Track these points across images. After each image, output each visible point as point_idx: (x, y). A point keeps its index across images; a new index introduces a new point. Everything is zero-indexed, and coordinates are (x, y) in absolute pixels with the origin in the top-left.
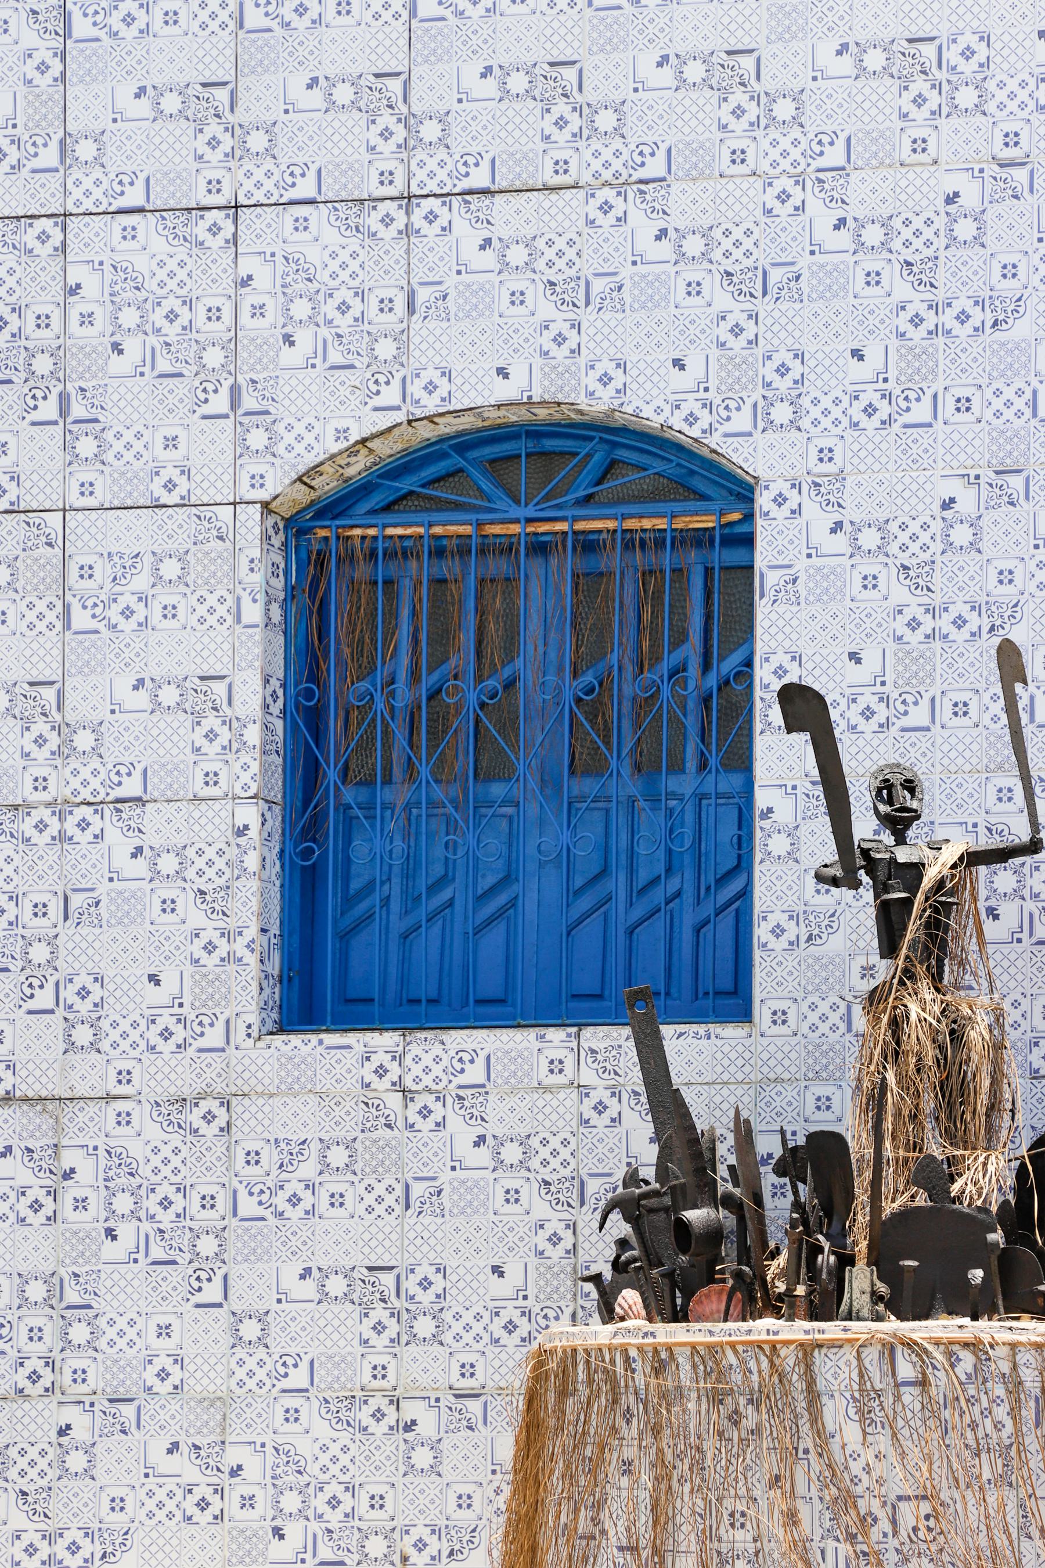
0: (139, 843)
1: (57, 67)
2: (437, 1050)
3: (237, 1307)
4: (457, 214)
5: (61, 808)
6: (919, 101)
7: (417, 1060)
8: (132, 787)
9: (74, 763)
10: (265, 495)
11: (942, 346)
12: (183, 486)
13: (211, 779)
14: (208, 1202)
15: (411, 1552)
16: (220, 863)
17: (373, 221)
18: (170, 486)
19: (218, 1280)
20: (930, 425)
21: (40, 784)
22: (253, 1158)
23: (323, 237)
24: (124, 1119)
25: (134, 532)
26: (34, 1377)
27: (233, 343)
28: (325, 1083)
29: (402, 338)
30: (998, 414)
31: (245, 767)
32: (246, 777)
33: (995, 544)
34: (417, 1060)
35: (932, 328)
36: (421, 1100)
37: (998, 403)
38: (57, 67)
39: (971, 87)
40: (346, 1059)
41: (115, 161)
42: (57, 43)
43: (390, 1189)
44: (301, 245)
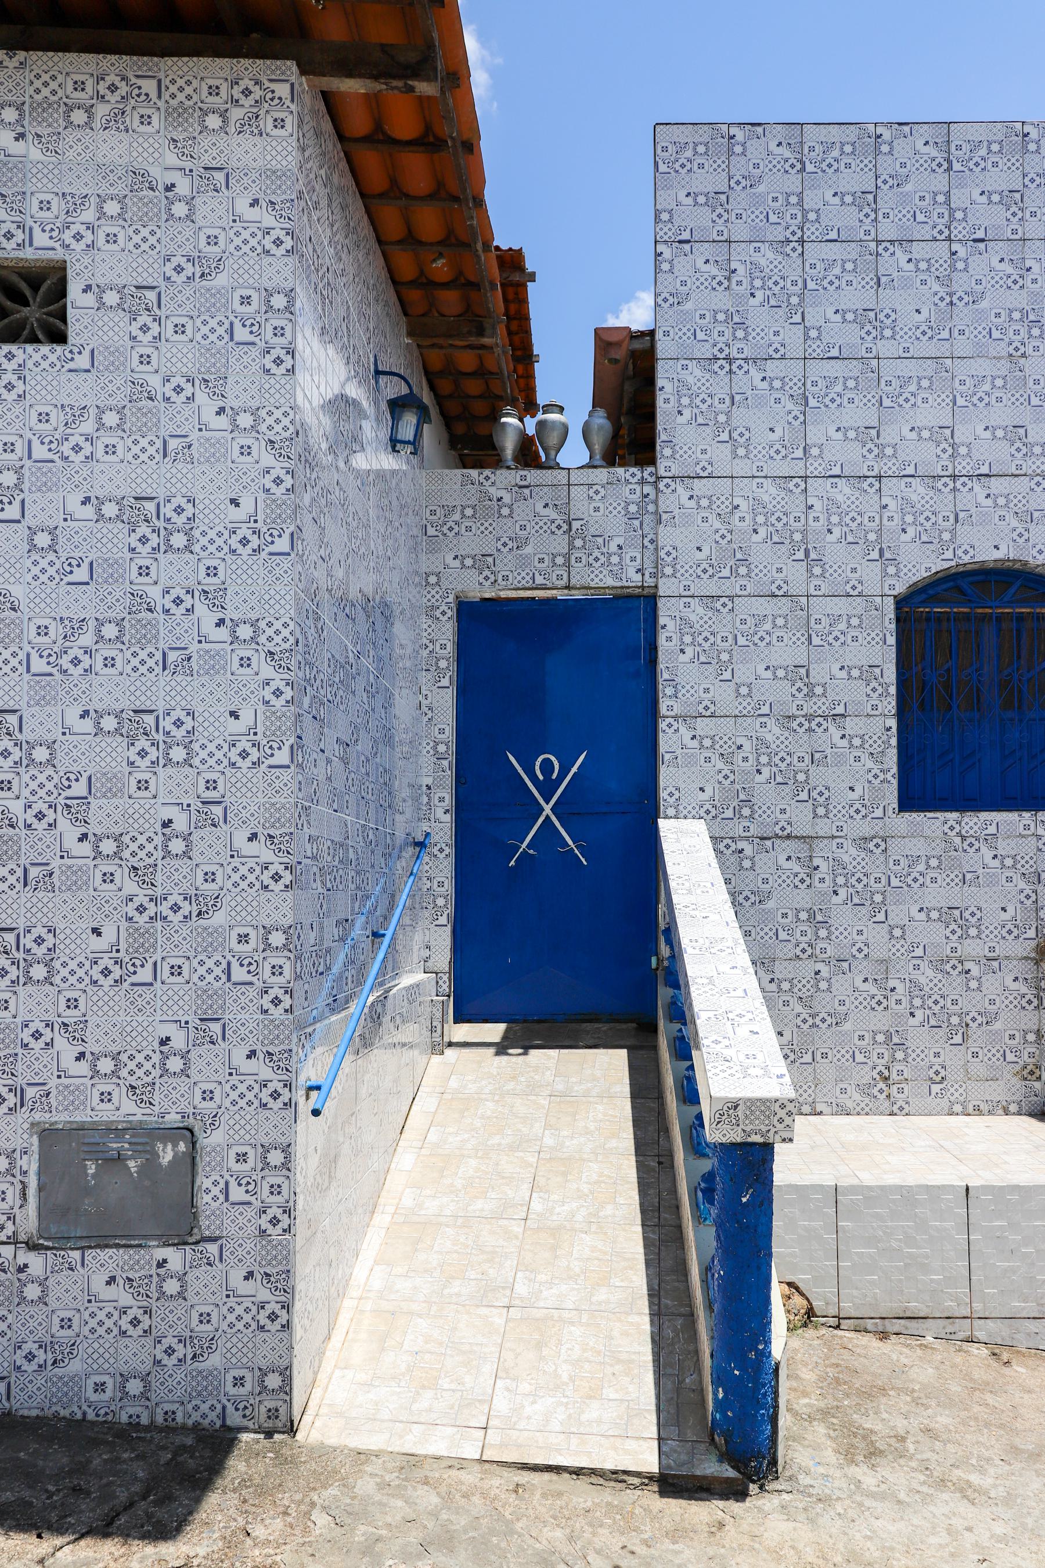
0: (82, 1049)
1: (802, 418)
2: (975, 820)
3: (891, 923)
5: (809, 718)
8: (840, 710)
9: (814, 699)
10: (895, 593)
11: (160, 928)
12: (860, 588)
13: (875, 707)
14: (878, 880)
16: (879, 742)
17: (940, 485)
18: (854, 588)
20: (151, 984)
21: (800, 707)
22: (897, 863)
23: (918, 491)
26: (804, 951)
27: (879, 531)
28: (928, 833)
29: (953, 532)
30: (202, 978)
32: (890, 707)
33: (200, 1071)
36: (969, 840)
38: (802, 418)
41: (828, 456)
42: (802, 408)
44: (909, 493)
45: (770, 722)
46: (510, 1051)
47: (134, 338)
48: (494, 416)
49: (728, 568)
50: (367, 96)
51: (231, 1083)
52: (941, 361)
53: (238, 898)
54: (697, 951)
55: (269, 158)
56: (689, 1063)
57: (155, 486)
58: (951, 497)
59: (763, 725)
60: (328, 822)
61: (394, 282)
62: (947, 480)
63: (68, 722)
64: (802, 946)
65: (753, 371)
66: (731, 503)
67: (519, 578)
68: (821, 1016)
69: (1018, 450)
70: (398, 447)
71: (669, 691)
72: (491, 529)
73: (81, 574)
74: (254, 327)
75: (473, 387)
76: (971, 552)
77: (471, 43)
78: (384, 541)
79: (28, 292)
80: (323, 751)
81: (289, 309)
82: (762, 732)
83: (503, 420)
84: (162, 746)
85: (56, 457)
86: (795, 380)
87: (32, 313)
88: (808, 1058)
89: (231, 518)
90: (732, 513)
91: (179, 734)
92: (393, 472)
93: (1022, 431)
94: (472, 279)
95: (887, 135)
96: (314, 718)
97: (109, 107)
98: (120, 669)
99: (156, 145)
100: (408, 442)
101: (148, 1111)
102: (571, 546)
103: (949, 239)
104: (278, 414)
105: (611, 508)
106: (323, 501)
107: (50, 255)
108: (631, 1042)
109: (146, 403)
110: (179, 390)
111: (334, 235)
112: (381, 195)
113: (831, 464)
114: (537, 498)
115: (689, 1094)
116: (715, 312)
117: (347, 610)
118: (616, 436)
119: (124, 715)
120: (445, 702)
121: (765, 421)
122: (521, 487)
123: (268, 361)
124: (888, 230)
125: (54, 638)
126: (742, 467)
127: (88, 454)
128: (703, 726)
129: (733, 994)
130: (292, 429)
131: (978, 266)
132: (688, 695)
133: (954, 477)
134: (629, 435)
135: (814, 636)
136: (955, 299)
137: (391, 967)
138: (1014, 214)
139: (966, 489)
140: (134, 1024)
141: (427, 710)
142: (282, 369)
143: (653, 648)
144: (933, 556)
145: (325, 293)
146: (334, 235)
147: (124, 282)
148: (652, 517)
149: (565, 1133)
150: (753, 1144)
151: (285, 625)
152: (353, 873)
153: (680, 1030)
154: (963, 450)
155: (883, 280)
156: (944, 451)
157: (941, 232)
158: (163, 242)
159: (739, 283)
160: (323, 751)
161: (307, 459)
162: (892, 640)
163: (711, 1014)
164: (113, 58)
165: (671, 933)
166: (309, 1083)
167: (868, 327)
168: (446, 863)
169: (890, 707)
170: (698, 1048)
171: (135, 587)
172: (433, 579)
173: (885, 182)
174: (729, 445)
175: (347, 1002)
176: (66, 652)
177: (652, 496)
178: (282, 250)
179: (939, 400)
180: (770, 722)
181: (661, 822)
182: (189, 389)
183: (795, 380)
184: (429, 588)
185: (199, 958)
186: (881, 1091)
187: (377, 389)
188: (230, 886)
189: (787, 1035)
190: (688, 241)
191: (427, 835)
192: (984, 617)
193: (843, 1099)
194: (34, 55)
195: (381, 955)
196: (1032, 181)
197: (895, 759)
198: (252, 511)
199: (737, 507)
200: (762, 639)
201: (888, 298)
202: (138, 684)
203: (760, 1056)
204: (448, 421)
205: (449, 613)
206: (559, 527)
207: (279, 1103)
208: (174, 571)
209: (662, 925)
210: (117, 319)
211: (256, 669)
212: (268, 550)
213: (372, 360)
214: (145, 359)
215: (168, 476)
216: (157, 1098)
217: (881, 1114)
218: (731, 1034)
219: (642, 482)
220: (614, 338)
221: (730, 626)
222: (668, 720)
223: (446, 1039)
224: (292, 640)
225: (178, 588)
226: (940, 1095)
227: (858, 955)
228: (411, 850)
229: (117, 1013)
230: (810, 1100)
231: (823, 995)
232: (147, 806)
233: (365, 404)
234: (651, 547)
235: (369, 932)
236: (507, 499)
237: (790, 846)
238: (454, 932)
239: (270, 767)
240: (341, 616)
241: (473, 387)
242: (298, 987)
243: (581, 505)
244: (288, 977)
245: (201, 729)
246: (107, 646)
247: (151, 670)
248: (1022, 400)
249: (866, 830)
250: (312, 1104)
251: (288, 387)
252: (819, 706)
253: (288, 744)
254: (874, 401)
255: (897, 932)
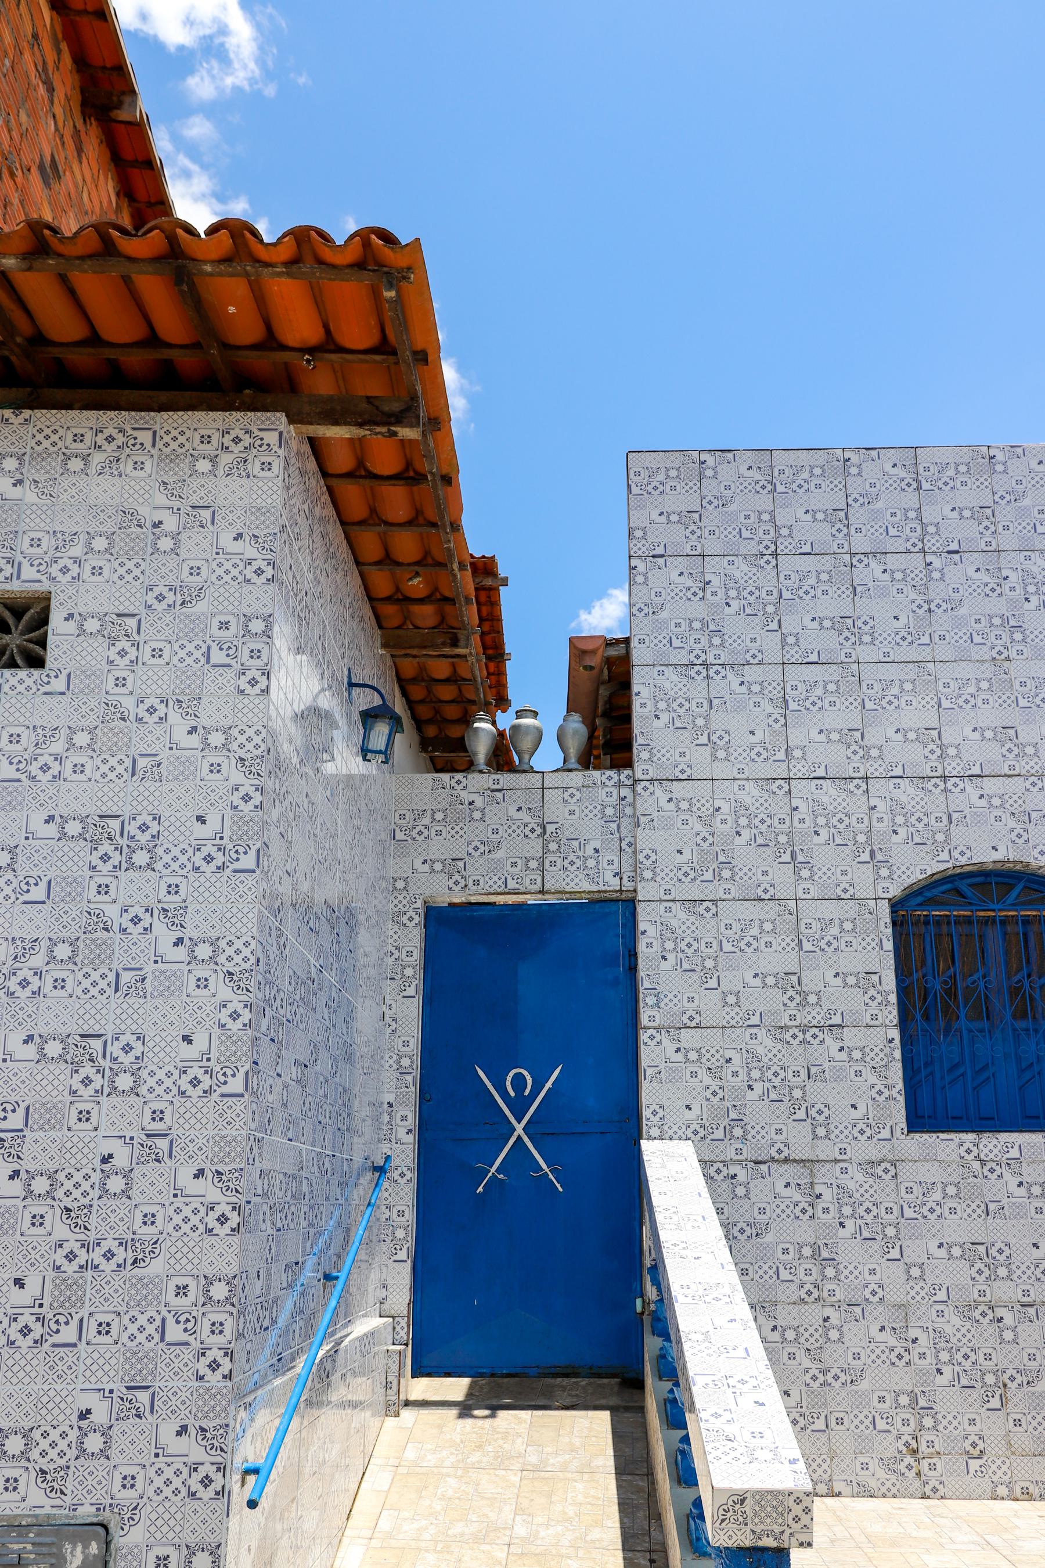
1: (782, 721)
2: (995, 1141)
3: (908, 1261)
4: (967, 784)
5: (804, 1028)
6: (86, 1082)
7: (985, 1146)
8: (836, 1020)
9: (808, 1009)
10: (890, 896)
11: (90, 1279)
14: (889, 1211)
15: (1008, 1382)
16: (882, 1055)
19: (897, 1248)
20: (75, 1345)
21: (793, 1017)
22: (909, 1190)
24: (844, 1171)
25: (830, 910)
26: (809, 1293)
27: (869, 833)
28: (942, 1156)
29: (947, 833)
31: (890, 1012)
32: (891, 1017)
33: (142, 1192)
34: (985, 1146)
35: (83, 1263)
36: (989, 1165)
37: (133, 1329)
38: (782, 721)
39: (128, 1074)
40: (950, 1146)
43: (978, 1206)
44: (897, 794)
45: (762, 1034)
46: (476, 1412)
47: (74, 1093)
48: (466, 720)
49: (711, 871)
50: (351, 440)
51: (176, 1205)
52: (922, 665)
53: (180, 1244)
54: (689, 1300)
55: (255, 496)
56: (683, 1433)
57: (121, 804)
58: (942, 798)
59: (753, 1037)
60: (280, 1153)
61: (371, 599)
62: (937, 780)
63: (32, 827)
64: (807, 1287)
65: (731, 676)
66: (712, 805)
67: (491, 882)
68: (833, 1372)
69: (1010, 750)
70: (369, 756)
71: (651, 1000)
72: (461, 833)
73: (38, 893)
74: (230, 649)
75: (446, 693)
76: (968, 854)
77: (449, 373)
78: (351, 849)
79: (10, 620)
80: (279, 1075)
81: (267, 633)
82: (753, 1045)
83: (476, 725)
84: (108, 1073)
85: (23, 777)
86: (774, 684)
87: (13, 640)
88: (820, 1424)
89: (196, 835)
90: (713, 815)
91: (143, 838)
92: (364, 778)
93: (1012, 732)
94: (447, 594)
95: (855, 458)
96: (273, 1040)
97: (105, 455)
98: (70, 991)
99: (147, 488)
100: (380, 752)
101: (58, 1502)
102: (545, 849)
103: (923, 551)
104: (250, 732)
105: (587, 811)
106: (292, 815)
107: (36, 587)
108: (614, 1401)
109: (102, 935)
110: (152, 710)
111: (314, 561)
112: (361, 523)
113: (815, 766)
114: (510, 801)
115: (685, 1474)
116: (691, 621)
117: (311, 924)
118: (591, 737)
119: (89, 820)
120: (409, 1013)
121: (745, 724)
122: (493, 791)
123: (202, 1366)
124: (860, 543)
125: (25, 745)
126: (721, 770)
127: (36, 989)
128: (688, 1038)
129: (733, 1354)
130: (263, 747)
131: (955, 576)
132: (671, 1005)
133: (944, 778)
134: (604, 736)
135: (804, 941)
136: (933, 606)
137: (344, 1314)
138: (987, 528)
139: (958, 789)
140: (52, 1393)
141: (391, 1023)
142: (257, 690)
143: (632, 955)
144: (928, 858)
145: (302, 615)
146: (314, 561)
147: (106, 610)
148: (630, 820)
149: (538, 1520)
150: (764, 1549)
151: (247, 944)
152: (306, 1209)
153: (671, 1391)
154: (952, 751)
155: (859, 589)
156: (932, 752)
157: (914, 545)
158: (147, 573)
159: (714, 593)
160: (279, 1075)
161: (279, 768)
162: (889, 945)
163: (708, 1379)
164: (112, 414)
165: (657, 1271)
166: (245, 1465)
167: (846, 633)
168: (407, 1190)
169: (891, 1017)
170: (693, 1408)
171: (92, 906)
172: (400, 884)
173: (856, 500)
174: (708, 748)
175: (293, 1360)
176: (14, 974)
177: (630, 799)
178: (263, 579)
179: (923, 702)
180: (762, 1034)
181: (644, 1144)
182: (162, 710)
183: (774, 684)
184: (396, 894)
185: (131, 1314)
186: (909, 1467)
187: (350, 701)
188: (170, 1230)
189: (795, 1394)
190: (662, 556)
191: (388, 1158)
192: (987, 921)
193: (864, 1477)
194: (38, 413)
195: (333, 1303)
196: (1002, 498)
197: (900, 1073)
198: (205, 1048)
199: (718, 809)
200: (749, 945)
201: (865, 607)
202: (106, 789)
203: (767, 1434)
204: (419, 724)
205: (417, 919)
206: (533, 831)
207: (210, 1493)
208: (135, 889)
209: (648, 1263)
210: (95, 645)
211: (213, 990)
212: (232, 867)
213: (346, 673)
214: (103, 889)
215: (135, 794)
216: (69, 1486)
217: (912, 1496)
218: (732, 1406)
219: (619, 785)
220: (589, 646)
221: (714, 931)
222: (650, 1032)
223: (402, 1397)
224: (253, 960)
225: (137, 907)
226: (980, 1473)
227: (872, 1299)
228: (369, 1176)
229: (33, 1380)
230: (826, 1477)
231: (834, 1346)
232: (86, 1140)
233: (337, 716)
234: (629, 850)
235: (320, 1275)
236: (479, 803)
237: (788, 1172)
238: (414, 1268)
239: (235, 871)
240: (305, 929)
241: (446, 693)
242: (240, 1348)
243: (555, 809)
244: (229, 1337)
245: (150, 1055)
246: (58, 967)
247: (102, 992)
248: (1009, 702)
249: (874, 1154)
250: (248, 1492)
251: (261, 706)
252: (814, 1016)
253: (243, 1071)
254: (856, 704)
255: (915, 1272)
